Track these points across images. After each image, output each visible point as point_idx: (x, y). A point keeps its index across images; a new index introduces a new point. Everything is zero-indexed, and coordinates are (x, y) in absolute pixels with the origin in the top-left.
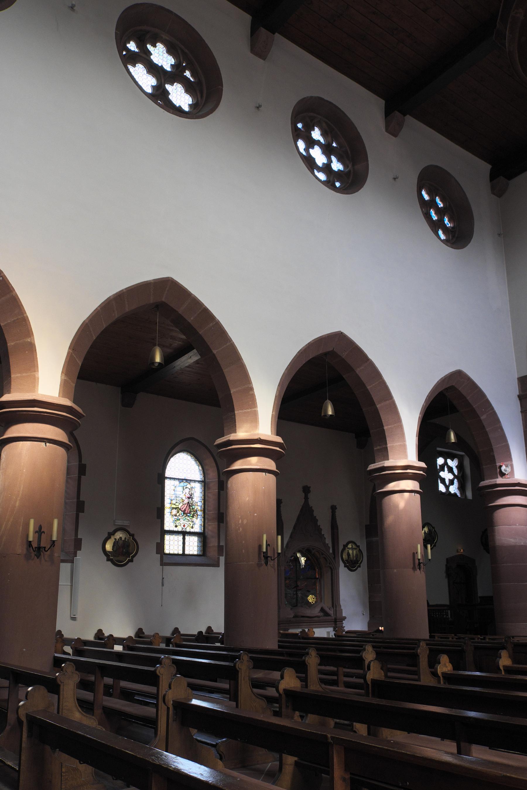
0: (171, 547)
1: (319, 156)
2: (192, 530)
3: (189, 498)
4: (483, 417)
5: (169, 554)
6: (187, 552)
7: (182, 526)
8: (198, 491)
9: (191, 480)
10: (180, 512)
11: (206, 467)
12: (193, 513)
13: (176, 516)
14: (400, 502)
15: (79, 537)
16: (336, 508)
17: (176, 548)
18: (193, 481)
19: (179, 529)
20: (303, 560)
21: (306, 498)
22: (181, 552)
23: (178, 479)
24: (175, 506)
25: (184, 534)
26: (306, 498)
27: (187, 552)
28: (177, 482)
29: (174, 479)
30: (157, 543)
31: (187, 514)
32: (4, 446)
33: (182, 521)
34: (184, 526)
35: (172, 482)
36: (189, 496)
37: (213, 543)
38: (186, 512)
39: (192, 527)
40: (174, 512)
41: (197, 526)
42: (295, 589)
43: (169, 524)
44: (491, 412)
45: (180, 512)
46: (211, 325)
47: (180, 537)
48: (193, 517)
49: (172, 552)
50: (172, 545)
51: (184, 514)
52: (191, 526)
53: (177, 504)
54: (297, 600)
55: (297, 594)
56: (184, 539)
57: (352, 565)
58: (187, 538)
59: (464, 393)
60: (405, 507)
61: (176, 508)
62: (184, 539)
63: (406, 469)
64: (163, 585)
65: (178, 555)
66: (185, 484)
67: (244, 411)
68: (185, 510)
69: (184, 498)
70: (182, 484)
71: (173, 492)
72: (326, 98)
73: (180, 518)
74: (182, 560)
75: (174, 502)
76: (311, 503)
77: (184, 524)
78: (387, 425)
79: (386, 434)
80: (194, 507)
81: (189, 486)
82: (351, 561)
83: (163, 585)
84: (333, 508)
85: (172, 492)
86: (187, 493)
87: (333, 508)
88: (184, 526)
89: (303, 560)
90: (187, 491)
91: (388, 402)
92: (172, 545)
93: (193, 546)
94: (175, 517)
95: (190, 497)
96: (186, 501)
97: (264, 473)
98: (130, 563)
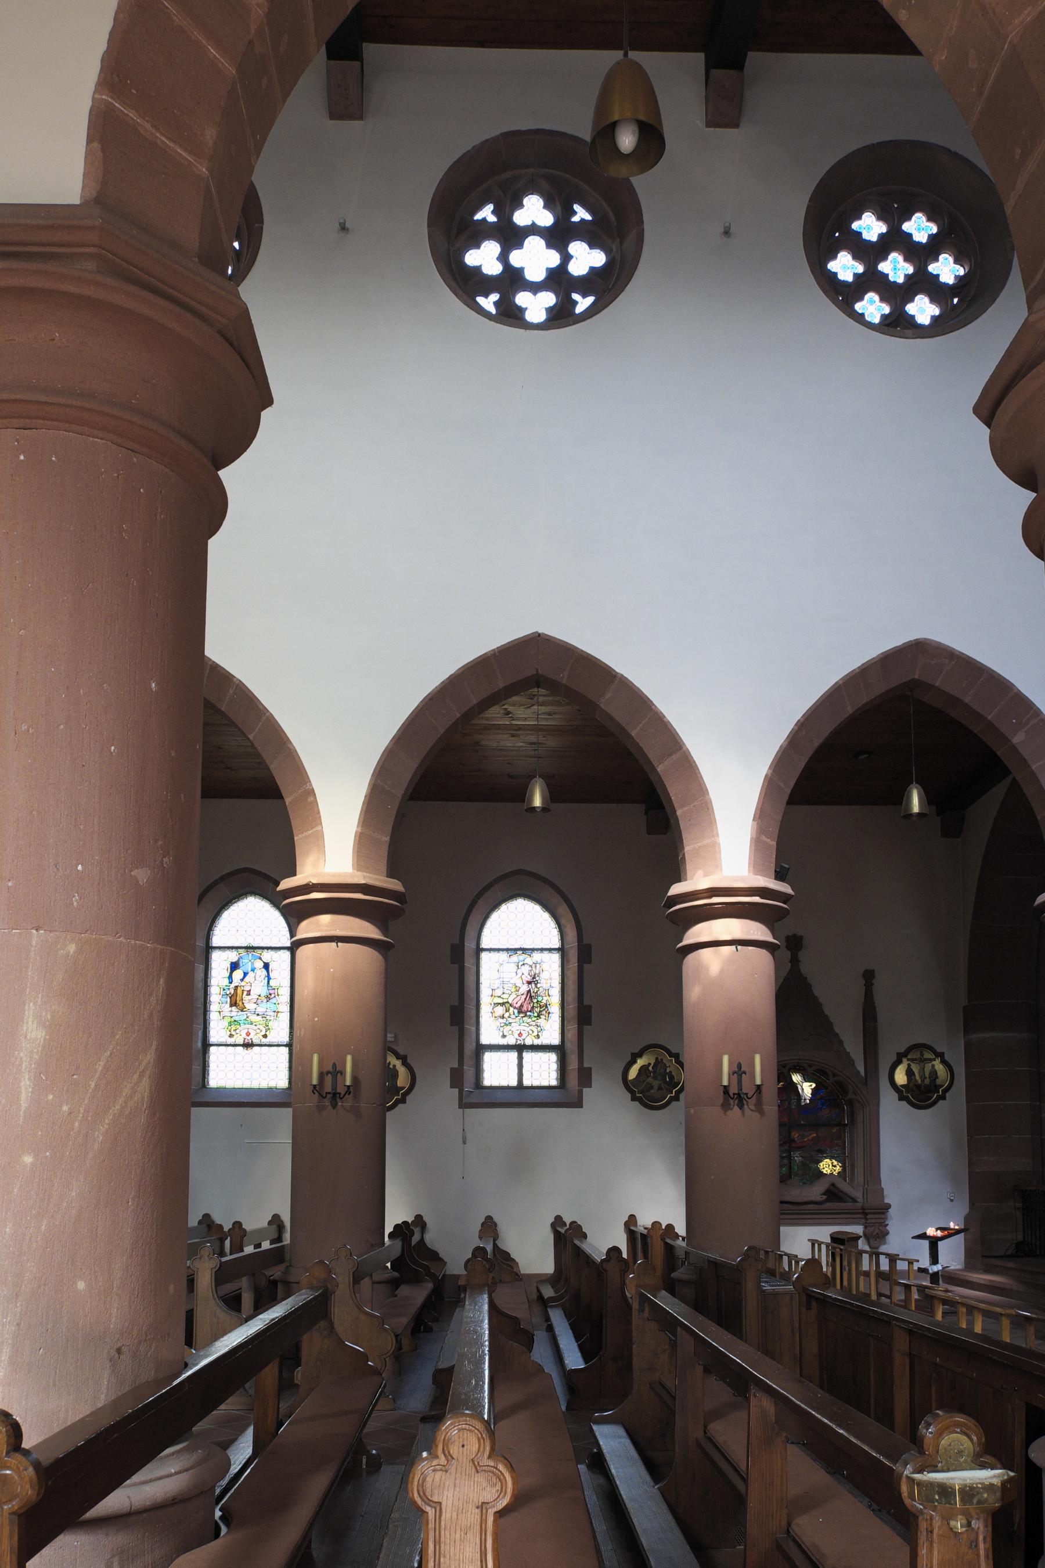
0: (536, 1075)
1: (535, 259)
2: (537, 1042)
3: (529, 983)
4: (1017, 739)
5: (532, 1088)
6: (527, 1082)
7: (517, 1036)
8: (550, 969)
9: (533, 950)
10: (511, 1009)
11: (563, 922)
12: (537, 1010)
13: (503, 1017)
14: (711, 963)
15: (586, 1065)
16: (873, 976)
17: (545, 1075)
18: (537, 950)
19: (511, 1041)
20: (807, 1089)
21: (795, 961)
22: (514, 1083)
23: (507, 950)
24: (501, 1001)
25: (520, 1049)
26: (795, 961)
27: (527, 1082)
28: (504, 956)
29: (498, 950)
30: (451, 1069)
31: (525, 1013)
32: (496, 906)
33: (516, 1027)
34: (520, 1035)
35: (493, 954)
36: (529, 979)
37: (573, 1064)
38: (525, 1008)
39: (538, 1037)
40: (500, 1010)
41: (551, 1032)
42: (786, 1147)
43: (489, 1033)
44: (1032, 723)
45: (511, 1009)
46: (231, 692)
47: (513, 1055)
48: (539, 1016)
49: (536, 1083)
50: (498, 1070)
51: (519, 1013)
52: (535, 1034)
53: (505, 996)
54: (790, 1168)
55: (789, 1157)
56: (520, 1059)
57: (921, 1095)
58: (527, 1056)
59: (956, 693)
60: (722, 971)
61: (503, 1004)
62: (520, 1059)
63: (710, 897)
64: (464, 1143)
65: (508, 1088)
66: (522, 957)
67: (305, 834)
68: (522, 1006)
69: (519, 984)
70: (515, 958)
71: (496, 975)
72: (524, 127)
73: (510, 1020)
74: (520, 1097)
75: (498, 992)
76: (805, 969)
77: (520, 1030)
78: (682, 806)
79: (682, 826)
80: (540, 999)
81: (529, 961)
82: (918, 1087)
83: (464, 1143)
84: (869, 976)
85: (496, 977)
86: (526, 974)
87: (869, 976)
88: (520, 1035)
89: (807, 1089)
90: (525, 969)
91: (675, 757)
92: (498, 1070)
93: (542, 1071)
94: (501, 1020)
95: (533, 981)
96: (524, 988)
97: (334, 944)
98: (400, 1106)
